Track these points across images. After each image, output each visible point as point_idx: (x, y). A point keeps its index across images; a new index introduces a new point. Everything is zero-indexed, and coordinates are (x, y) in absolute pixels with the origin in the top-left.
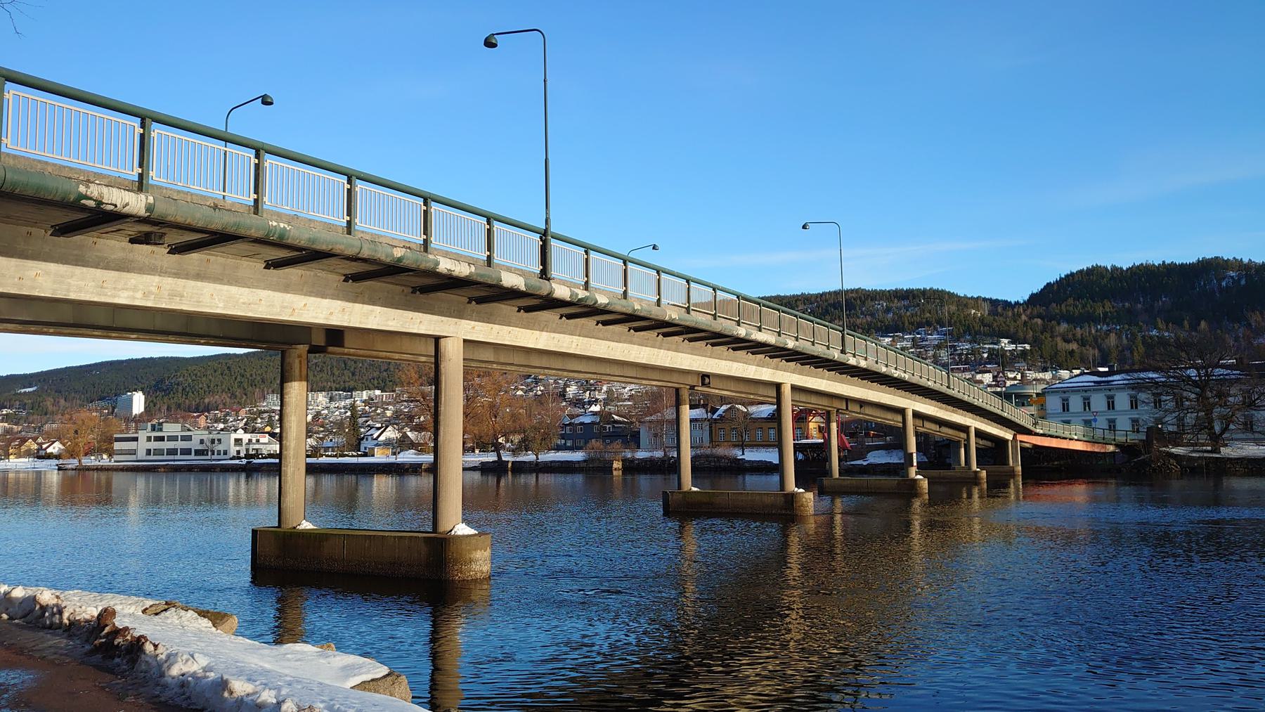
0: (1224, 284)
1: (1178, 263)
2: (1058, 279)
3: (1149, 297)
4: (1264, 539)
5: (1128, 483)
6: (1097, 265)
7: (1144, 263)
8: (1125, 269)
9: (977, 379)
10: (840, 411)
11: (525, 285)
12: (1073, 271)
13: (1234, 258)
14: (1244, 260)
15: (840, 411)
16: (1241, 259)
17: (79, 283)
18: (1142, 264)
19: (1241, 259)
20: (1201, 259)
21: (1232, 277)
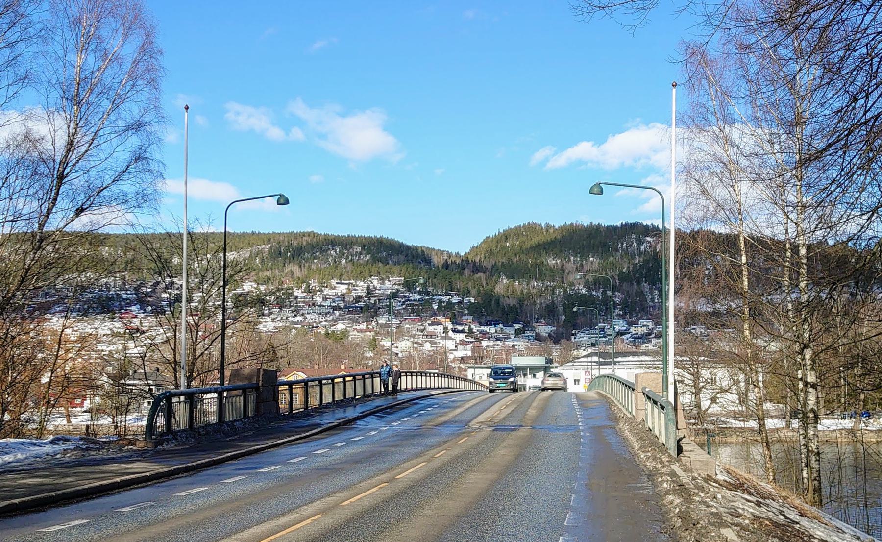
0: (642, 248)
1: (603, 225)
2: (497, 234)
3: (579, 256)
4: (881, 123)
5: (589, 164)
6: (532, 222)
7: (574, 223)
8: (557, 227)
9: (430, 330)
10: (324, 382)
11: (108, 234)
12: (510, 227)
13: (652, 224)
14: (659, 227)
15: (324, 382)
16: (658, 226)
17: (37, 441)
18: (572, 224)
19: (658, 226)
20: (624, 223)
21: (649, 242)
